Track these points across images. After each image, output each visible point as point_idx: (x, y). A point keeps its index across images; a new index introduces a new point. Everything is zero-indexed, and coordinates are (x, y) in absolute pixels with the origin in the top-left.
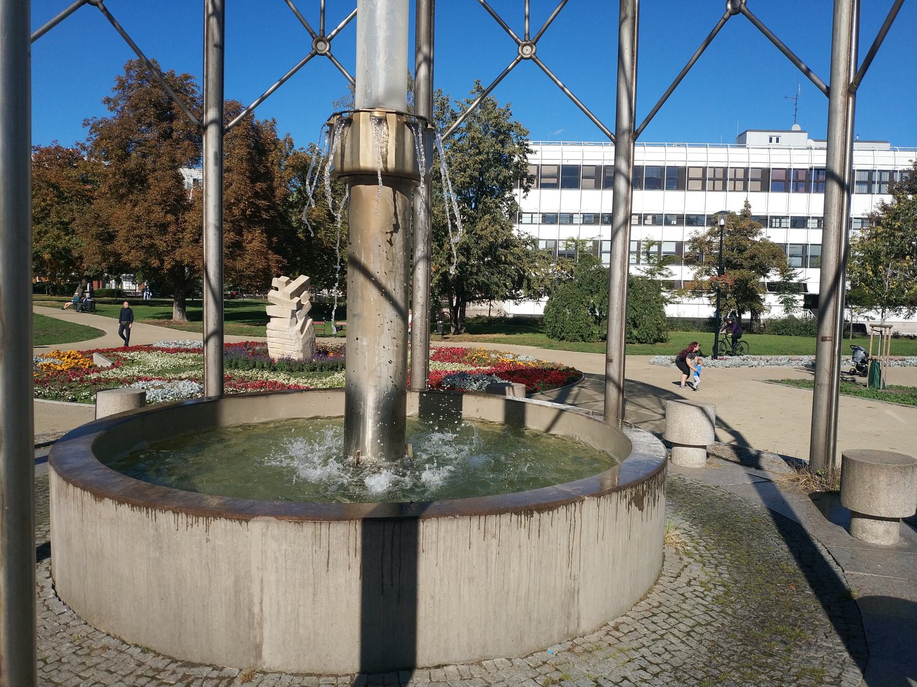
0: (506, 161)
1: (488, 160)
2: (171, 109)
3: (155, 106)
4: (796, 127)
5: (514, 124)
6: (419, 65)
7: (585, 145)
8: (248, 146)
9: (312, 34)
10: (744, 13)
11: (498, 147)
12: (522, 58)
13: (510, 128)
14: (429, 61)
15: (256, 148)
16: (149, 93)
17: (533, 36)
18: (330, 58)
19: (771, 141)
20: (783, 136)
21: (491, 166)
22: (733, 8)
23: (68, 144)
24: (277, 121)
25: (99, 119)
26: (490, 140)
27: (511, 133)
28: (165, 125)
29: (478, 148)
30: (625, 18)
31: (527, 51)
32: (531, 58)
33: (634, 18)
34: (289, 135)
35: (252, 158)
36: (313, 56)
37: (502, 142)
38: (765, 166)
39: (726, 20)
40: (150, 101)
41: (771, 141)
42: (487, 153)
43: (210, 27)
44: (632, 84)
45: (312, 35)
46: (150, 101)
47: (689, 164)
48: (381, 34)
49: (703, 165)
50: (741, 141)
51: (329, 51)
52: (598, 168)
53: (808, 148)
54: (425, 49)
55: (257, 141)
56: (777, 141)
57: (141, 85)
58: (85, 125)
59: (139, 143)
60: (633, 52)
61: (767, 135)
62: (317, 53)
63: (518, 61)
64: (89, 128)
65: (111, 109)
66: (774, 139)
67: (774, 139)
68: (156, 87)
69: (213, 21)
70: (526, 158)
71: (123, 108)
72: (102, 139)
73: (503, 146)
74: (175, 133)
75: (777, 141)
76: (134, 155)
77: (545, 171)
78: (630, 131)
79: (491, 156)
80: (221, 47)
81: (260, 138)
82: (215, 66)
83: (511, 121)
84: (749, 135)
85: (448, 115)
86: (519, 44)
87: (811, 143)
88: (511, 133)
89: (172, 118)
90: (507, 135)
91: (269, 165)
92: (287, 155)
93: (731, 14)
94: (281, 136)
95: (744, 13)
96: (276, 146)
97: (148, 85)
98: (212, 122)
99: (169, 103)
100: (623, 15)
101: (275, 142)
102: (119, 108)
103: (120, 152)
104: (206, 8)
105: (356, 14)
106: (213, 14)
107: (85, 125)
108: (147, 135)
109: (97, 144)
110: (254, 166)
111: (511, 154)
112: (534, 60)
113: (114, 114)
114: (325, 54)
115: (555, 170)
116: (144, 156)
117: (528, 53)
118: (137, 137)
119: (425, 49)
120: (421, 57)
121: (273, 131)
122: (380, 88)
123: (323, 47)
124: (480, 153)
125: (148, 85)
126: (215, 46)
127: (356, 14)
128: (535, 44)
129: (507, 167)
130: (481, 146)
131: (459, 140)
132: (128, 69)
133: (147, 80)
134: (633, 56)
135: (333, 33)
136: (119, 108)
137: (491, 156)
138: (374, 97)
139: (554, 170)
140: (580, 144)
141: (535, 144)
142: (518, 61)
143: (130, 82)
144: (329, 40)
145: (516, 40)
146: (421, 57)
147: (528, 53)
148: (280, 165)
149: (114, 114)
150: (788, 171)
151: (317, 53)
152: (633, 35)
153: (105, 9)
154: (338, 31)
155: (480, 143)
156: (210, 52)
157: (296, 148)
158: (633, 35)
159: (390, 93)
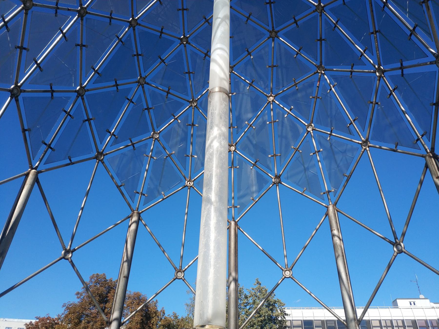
0: (274, 320)
1: (265, 320)
2: (108, 297)
3: (100, 296)
4: (422, 296)
5: (277, 300)
6: (231, 283)
7: (314, 309)
8: (142, 316)
9: (175, 268)
10: (405, 253)
11: (270, 312)
12: (285, 277)
13: (275, 302)
14: (236, 280)
15: (146, 316)
16: (98, 289)
17: (290, 266)
18: (183, 280)
19: (411, 304)
20: (417, 301)
21: (266, 323)
22: (398, 250)
23: (54, 316)
24: (158, 301)
25: (71, 303)
26: (265, 309)
27: (276, 305)
28: (102, 305)
29: (259, 313)
30: (339, 256)
31: (288, 274)
32: (290, 277)
33: (343, 256)
34: (163, 308)
35: (143, 321)
36: (175, 280)
37: (272, 310)
38: (413, 318)
39: (396, 256)
40: (98, 293)
41: (411, 304)
42: (264, 316)
43: (123, 267)
44: (350, 291)
45: (175, 269)
46: (98, 293)
47: (371, 318)
48: (212, 253)
49: (379, 318)
50: (395, 304)
51: (183, 277)
52: (323, 321)
53: (432, 308)
54: (233, 274)
55: (146, 312)
56: (414, 304)
57: (95, 286)
58: (63, 306)
59: (87, 316)
60: (346, 274)
61: (407, 301)
62: (177, 278)
63: (283, 279)
64: (65, 308)
65: (78, 298)
66: (412, 303)
67: (412, 303)
68: (102, 286)
69: (126, 264)
70: (285, 318)
71: (84, 297)
72: (69, 314)
73: (272, 312)
74: (106, 309)
75: (414, 304)
76: (83, 322)
77: (295, 323)
78: (355, 319)
79: (266, 317)
80: (127, 278)
81: (149, 311)
82: (122, 288)
83: (275, 298)
84: (398, 301)
85: (243, 296)
86: (283, 270)
87: (433, 305)
88: (276, 305)
89: (106, 302)
90: (273, 305)
91: (151, 325)
92: (161, 319)
93: (397, 253)
94: (159, 309)
95: (405, 253)
96: (156, 315)
97: (98, 286)
98: (115, 319)
99: (107, 294)
100: (337, 255)
101: (156, 313)
102: (82, 297)
103: (76, 321)
104: (123, 258)
105: (197, 258)
106: (126, 261)
107: (63, 306)
108: (93, 311)
109: (66, 316)
110: (143, 326)
111: (277, 316)
112: (292, 278)
113: (79, 300)
114: (181, 279)
115: (300, 323)
116: (89, 322)
117: (288, 274)
118: (88, 312)
119: (233, 274)
120: (231, 279)
121: (156, 306)
122: (209, 312)
123: (180, 275)
124: (260, 316)
125: (98, 286)
126: (124, 277)
127: (197, 258)
128: (291, 270)
129: (275, 323)
130: (261, 312)
131: (249, 309)
132: (91, 278)
133: (99, 284)
134: (347, 276)
135: (186, 268)
136: (82, 297)
137: (266, 317)
138: (205, 318)
139: (300, 323)
140: (311, 309)
141: (287, 309)
142: (283, 279)
143: (91, 284)
144: (184, 271)
145: (281, 268)
146: (231, 279)
147: (288, 274)
148: (157, 324)
149: (79, 300)
150: (426, 321)
151: (177, 278)
152: (345, 264)
153: (72, 261)
154: (189, 266)
155: (260, 311)
156: (121, 280)
157: (166, 315)
158: (345, 264)
159: (215, 315)
